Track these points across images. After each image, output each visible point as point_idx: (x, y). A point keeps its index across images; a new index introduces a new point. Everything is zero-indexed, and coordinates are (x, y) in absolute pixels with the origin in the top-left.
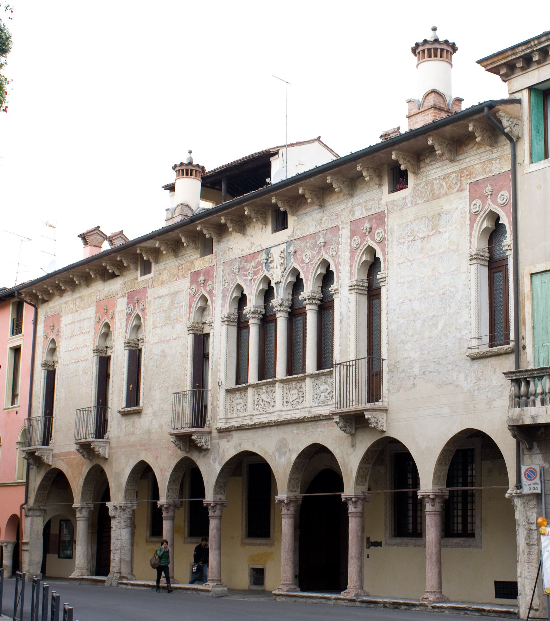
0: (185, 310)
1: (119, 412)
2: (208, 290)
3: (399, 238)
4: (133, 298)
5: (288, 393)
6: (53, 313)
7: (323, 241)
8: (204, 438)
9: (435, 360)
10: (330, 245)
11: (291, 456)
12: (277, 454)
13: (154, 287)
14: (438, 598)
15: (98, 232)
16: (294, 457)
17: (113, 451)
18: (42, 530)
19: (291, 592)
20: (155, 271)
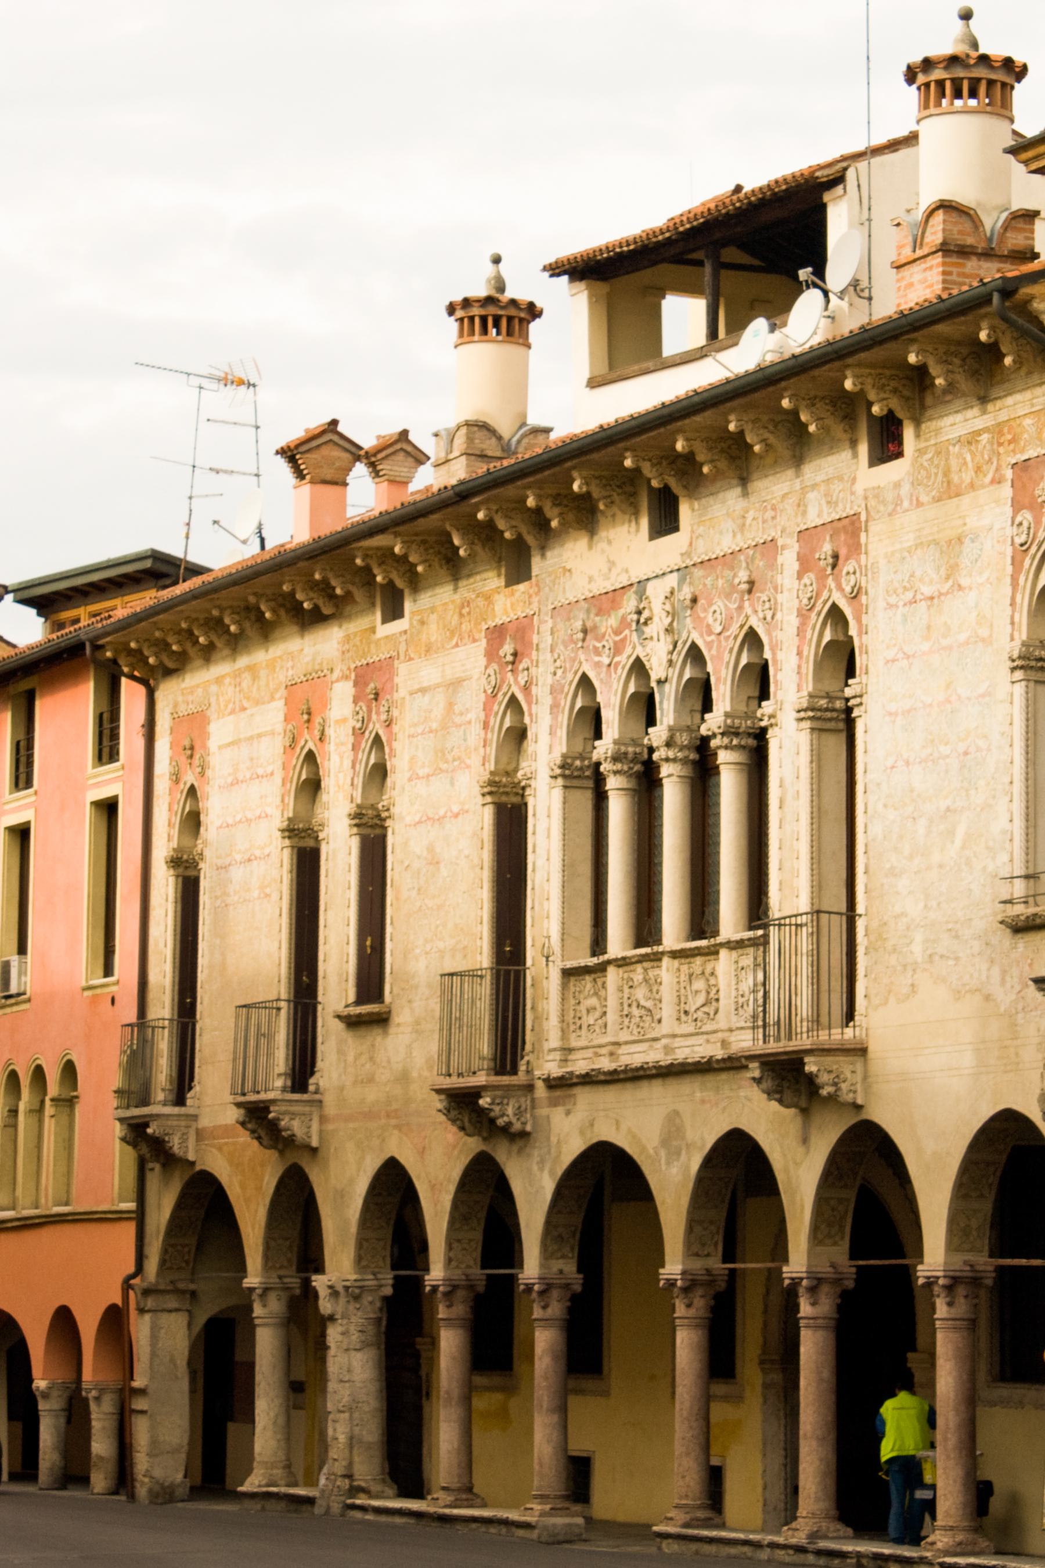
0: (475, 732)
1: (339, 1017)
2: (523, 683)
3: (887, 592)
4: (366, 684)
5: (688, 988)
6: (192, 708)
7: (745, 579)
8: (512, 1102)
9: (950, 926)
10: (762, 592)
11: (689, 1160)
12: (663, 1153)
13: (411, 659)
14: (960, 1544)
15: (335, 438)
16: (695, 1164)
17: (330, 1127)
18: (186, 1353)
19: (697, 1527)
20: (413, 613)
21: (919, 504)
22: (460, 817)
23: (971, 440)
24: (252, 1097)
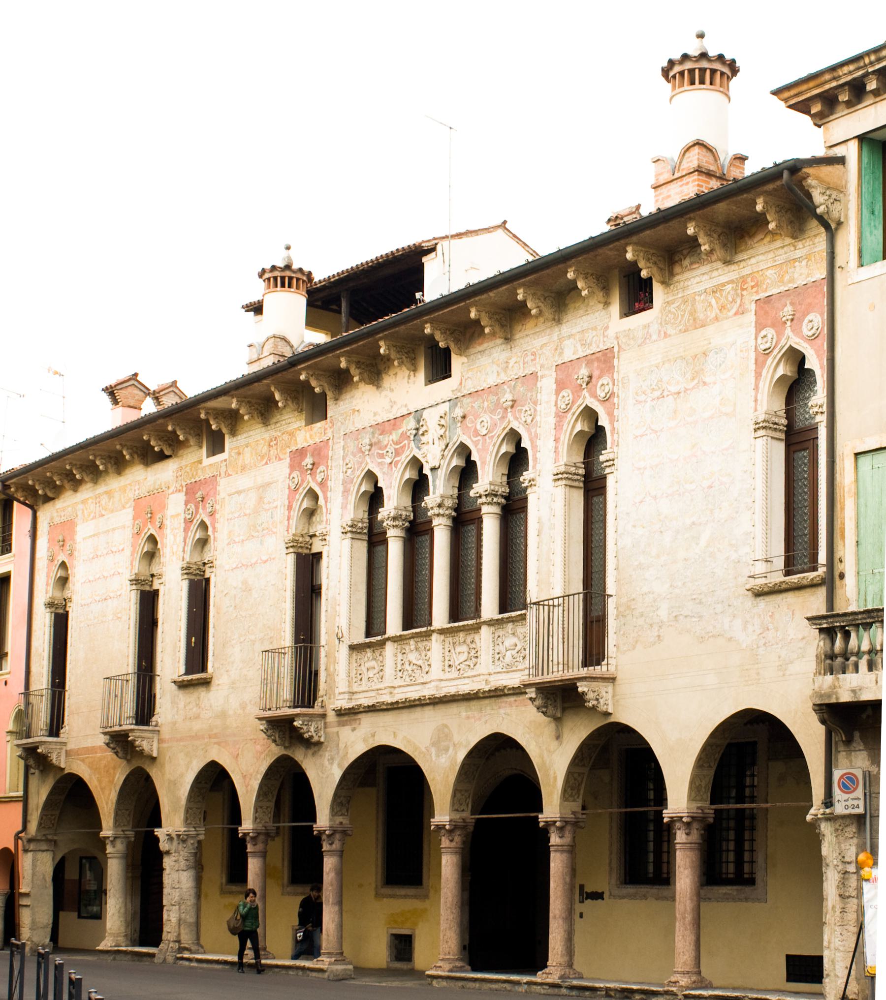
1: (175, 682)
4: (194, 493)
5: (452, 651)
7: (511, 398)
10: (522, 406)
11: (456, 753)
12: (433, 750)
13: (229, 475)
14: (694, 982)
15: (136, 383)
16: (461, 755)
17: (165, 745)
19: (456, 972)
20: (231, 449)
21: (666, 335)
22: (268, 563)
23: (716, 290)
24: (117, 728)
